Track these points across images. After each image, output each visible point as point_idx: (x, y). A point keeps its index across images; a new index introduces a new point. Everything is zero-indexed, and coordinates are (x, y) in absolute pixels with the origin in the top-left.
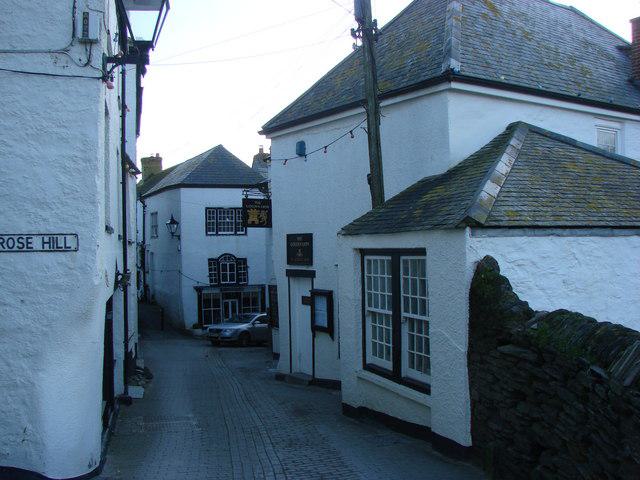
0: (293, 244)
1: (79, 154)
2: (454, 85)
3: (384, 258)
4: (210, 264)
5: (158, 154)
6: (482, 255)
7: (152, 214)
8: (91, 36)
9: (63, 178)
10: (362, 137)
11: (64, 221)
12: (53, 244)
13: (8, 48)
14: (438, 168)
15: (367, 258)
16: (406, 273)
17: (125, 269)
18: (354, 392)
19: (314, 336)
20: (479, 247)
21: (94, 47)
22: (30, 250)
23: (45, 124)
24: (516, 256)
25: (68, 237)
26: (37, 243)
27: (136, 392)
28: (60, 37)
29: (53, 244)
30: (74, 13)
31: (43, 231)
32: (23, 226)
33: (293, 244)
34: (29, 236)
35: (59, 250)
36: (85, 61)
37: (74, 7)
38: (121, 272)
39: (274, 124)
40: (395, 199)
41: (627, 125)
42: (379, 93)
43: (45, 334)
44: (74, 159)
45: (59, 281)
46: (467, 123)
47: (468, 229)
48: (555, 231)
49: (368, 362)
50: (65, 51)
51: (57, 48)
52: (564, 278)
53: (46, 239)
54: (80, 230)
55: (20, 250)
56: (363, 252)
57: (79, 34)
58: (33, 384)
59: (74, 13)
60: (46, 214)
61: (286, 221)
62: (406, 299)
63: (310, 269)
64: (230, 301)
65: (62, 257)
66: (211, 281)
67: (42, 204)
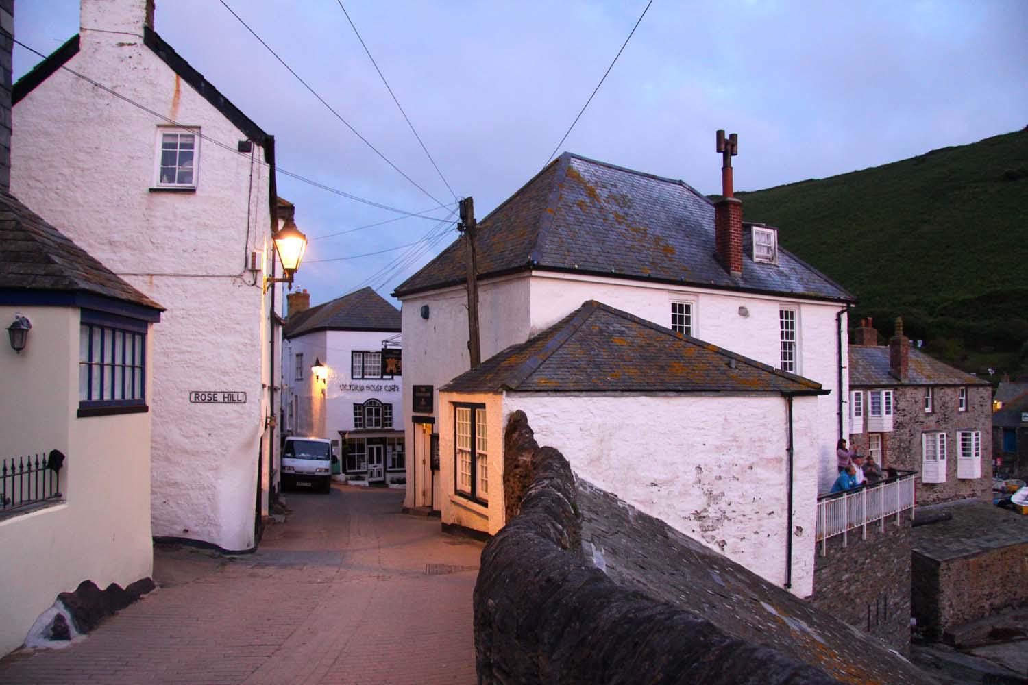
0: (419, 394)
1: (249, 342)
2: (534, 273)
3: (465, 409)
4: (355, 409)
5: (305, 291)
6: (515, 409)
7: (297, 355)
8: (257, 268)
9: (238, 357)
10: (464, 317)
11: (237, 383)
12: (230, 398)
13: (205, 274)
14: (522, 339)
15: (458, 408)
16: (479, 421)
17: (272, 414)
18: (450, 515)
19: (433, 474)
20: (511, 404)
21: (258, 274)
22: (216, 402)
23: (226, 322)
24: (541, 410)
25: (240, 395)
26: (220, 397)
27: (280, 518)
28: (237, 267)
29: (230, 398)
30: (246, 251)
31: (224, 390)
32: (211, 386)
33: (419, 394)
34: (215, 393)
35: (234, 402)
36: (252, 282)
37: (247, 248)
38: (269, 415)
39: (404, 289)
40: (488, 362)
41: (701, 297)
42: (480, 271)
43: (224, 455)
44: (244, 344)
45: (234, 422)
46: (550, 300)
47: (504, 393)
48: (572, 393)
49: (458, 488)
50: (240, 276)
51: (235, 274)
52: (581, 426)
53: (226, 395)
54: (246, 390)
55: (209, 402)
56: (456, 405)
57: (250, 266)
58: (215, 487)
59: (246, 251)
60: (226, 379)
61: (413, 374)
62: (479, 439)
63: (431, 416)
64: (375, 446)
65: (235, 406)
66: (356, 426)
67: (225, 373)
